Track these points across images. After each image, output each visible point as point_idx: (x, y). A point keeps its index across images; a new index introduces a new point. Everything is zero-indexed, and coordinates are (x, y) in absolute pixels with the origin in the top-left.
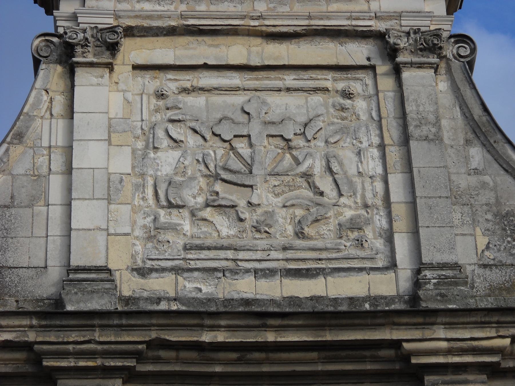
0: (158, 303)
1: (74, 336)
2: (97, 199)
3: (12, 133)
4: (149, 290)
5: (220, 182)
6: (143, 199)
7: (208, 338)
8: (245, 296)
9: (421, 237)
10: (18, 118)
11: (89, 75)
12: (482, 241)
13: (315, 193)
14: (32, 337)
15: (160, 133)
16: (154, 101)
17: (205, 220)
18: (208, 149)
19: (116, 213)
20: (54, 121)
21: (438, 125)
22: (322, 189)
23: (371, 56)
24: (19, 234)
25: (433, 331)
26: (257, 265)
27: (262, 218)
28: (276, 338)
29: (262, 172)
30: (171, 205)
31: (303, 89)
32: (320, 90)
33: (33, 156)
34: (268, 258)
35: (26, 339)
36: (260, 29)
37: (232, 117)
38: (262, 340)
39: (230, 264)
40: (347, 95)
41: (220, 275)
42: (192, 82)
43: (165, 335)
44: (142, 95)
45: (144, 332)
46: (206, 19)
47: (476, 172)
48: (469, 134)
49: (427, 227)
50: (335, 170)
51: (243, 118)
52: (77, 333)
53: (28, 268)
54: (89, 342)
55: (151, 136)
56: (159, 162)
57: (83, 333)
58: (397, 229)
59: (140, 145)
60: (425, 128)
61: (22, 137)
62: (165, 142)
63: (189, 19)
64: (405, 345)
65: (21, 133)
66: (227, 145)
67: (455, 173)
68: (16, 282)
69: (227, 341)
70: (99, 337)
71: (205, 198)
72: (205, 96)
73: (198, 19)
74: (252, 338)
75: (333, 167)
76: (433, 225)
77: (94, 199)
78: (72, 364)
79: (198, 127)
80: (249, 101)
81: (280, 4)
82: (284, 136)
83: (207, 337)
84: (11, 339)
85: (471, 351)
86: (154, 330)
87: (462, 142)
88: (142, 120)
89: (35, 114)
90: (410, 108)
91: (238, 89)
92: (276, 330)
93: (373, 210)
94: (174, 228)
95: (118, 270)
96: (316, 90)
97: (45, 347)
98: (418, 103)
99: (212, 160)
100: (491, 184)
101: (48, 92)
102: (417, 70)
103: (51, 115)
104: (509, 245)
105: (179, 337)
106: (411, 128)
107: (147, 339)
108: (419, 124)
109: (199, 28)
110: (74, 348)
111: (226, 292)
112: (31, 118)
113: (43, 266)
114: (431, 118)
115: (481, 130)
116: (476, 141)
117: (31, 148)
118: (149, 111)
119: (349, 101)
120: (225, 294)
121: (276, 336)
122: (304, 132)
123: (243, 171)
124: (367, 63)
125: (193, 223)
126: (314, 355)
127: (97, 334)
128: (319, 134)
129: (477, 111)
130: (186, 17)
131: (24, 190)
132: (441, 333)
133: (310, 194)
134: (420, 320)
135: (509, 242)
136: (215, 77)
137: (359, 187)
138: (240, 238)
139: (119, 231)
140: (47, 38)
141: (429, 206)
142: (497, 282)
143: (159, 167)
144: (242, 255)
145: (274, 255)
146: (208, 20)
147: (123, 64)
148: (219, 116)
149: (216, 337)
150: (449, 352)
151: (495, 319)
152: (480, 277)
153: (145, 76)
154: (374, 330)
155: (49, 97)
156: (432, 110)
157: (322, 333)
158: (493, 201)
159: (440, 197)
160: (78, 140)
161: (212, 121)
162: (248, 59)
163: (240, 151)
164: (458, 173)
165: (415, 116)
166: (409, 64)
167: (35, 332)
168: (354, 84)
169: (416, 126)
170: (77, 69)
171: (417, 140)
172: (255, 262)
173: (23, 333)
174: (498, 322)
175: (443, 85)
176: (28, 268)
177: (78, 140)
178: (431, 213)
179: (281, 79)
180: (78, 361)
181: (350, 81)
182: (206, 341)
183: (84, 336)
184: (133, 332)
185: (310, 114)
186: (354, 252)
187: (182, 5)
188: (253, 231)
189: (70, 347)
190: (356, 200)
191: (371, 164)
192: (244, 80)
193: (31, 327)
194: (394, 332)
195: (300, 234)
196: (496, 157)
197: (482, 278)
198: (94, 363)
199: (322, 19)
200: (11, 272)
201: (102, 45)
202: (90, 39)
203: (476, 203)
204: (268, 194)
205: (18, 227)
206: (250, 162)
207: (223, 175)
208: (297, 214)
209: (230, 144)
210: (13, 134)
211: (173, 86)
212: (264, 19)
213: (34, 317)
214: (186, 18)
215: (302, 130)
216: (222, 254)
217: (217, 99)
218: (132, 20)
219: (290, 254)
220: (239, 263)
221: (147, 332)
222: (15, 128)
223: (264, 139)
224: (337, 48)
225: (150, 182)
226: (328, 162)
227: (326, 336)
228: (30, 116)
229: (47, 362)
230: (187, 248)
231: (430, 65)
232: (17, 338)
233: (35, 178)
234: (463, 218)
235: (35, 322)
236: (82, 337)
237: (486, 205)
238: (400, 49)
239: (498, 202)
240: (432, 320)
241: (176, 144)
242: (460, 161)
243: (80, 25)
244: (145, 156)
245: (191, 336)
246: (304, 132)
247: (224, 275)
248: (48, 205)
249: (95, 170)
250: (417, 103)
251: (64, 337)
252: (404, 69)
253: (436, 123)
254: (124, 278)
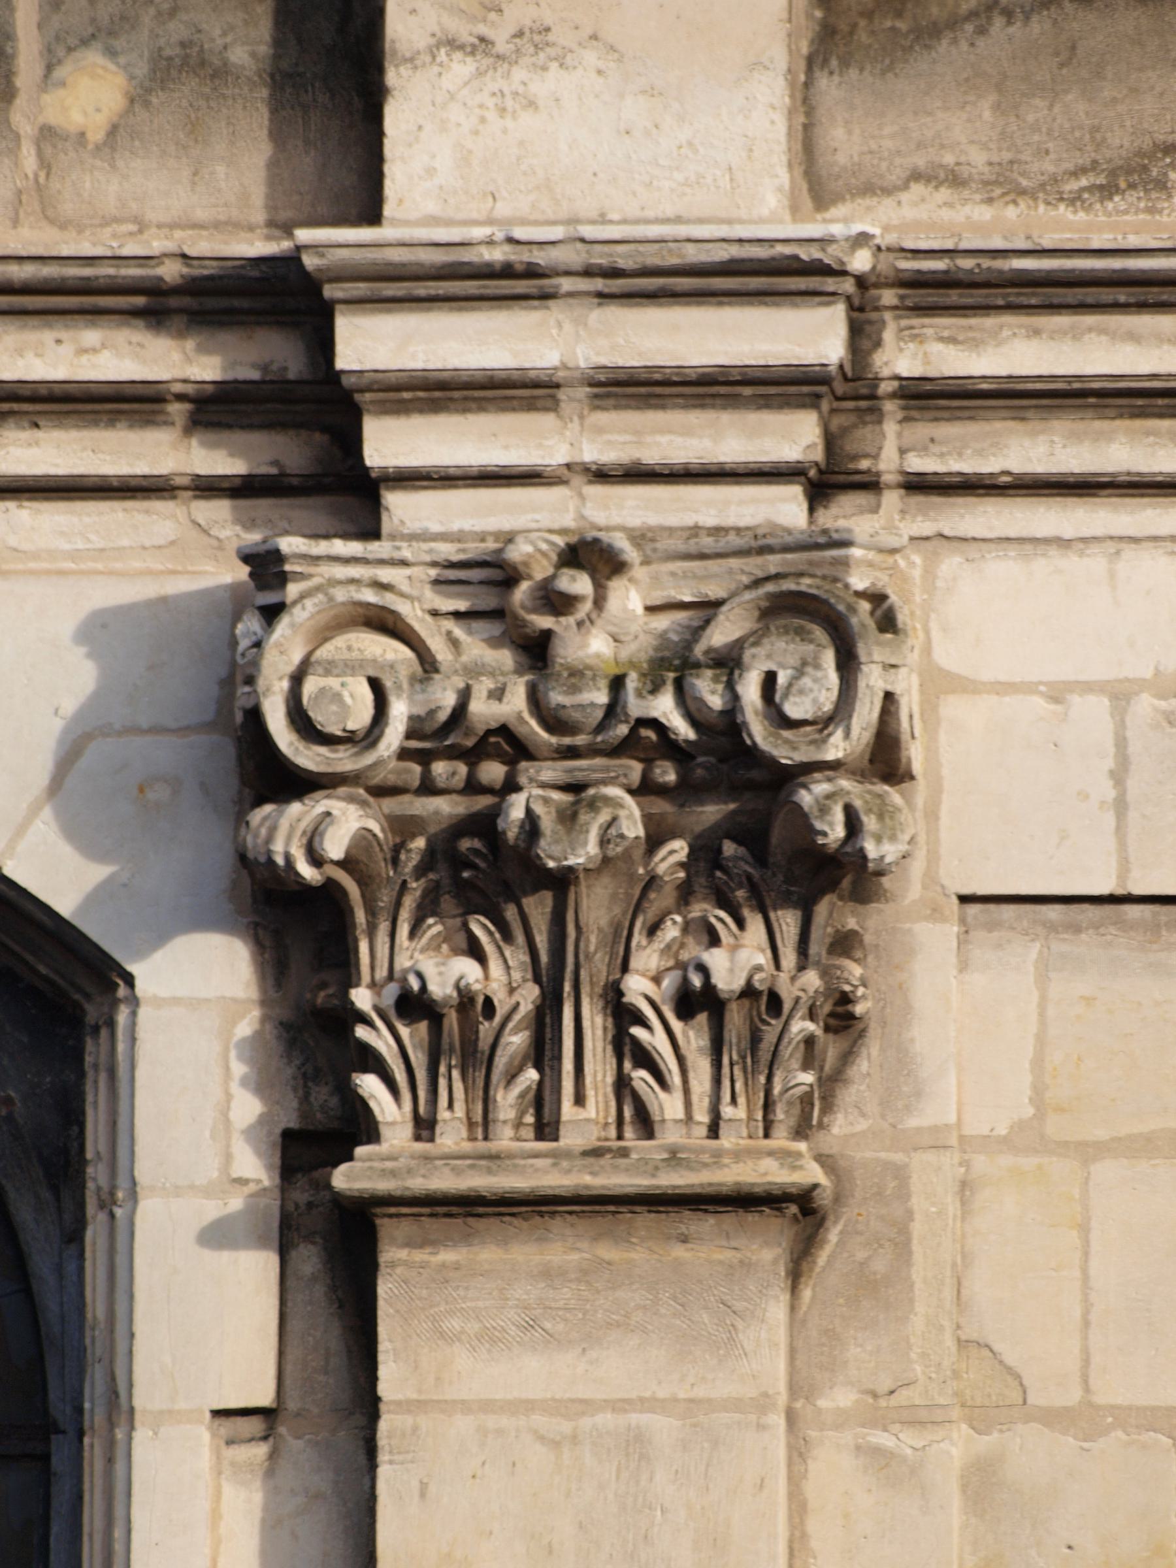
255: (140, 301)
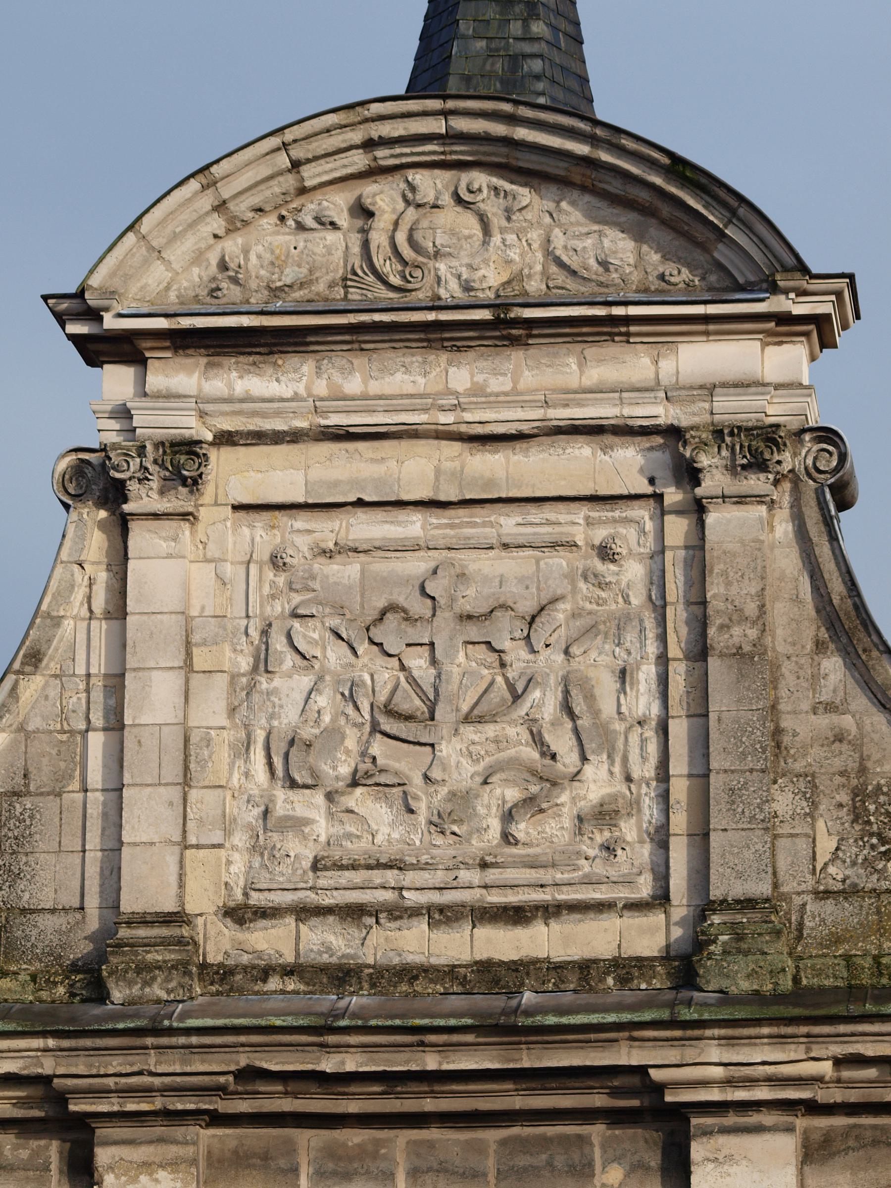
0: (265, 980)
1: (116, 1064)
2: (167, 784)
3: (21, 653)
4: (251, 951)
5: (378, 736)
6: (247, 774)
7: (330, 1065)
8: (410, 958)
9: (712, 850)
10: (33, 622)
11: (153, 536)
12: (826, 845)
13: (543, 754)
14: (48, 1066)
15: (279, 643)
16: (270, 574)
17: (350, 811)
18: (361, 670)
19: (199, 805)
20: (94, 624)
21: (760, 623)
22: (554, 748)
23: (657, 474)
24: (38, 846)
25: (699, 1051)
26: (436, 898)
27: (449, 807)
28: (440, 1064)
29: (452, 717)
30: (293, 784)
31: (533, 545)
32: (563, 545)
33: (61, 693)
34: (455, 884)
35: (40, 1071)
36: (455, 429)
37: (406, 605)
38: (418, 1068)
39: (388, 896)
40: (606, 553)
41: (371, 921)
42: (337, 534)
43: (261, 1060)
44: (249, 562)
45: (228, 1056)
46: (359, 414)
47: (830, 708)
48: (823, 629)
49: (722, 830)
50: (577, 711)
51: (421, 607)
52: (120, 1059)
53: (53, 911)
54: (140, 1073)
55: (263, 647)
56: (276, 700)
57: (130, 1058)
58: (675, 827)
59: (245, 663)
60: (736, 631)
61: (40, 660)
62: (290, 660)
63: (330, 414)
64: (652, 1072)
65: (39, 652)
66: (394, 662)
67: (788, 713)
68: (33, 938)
69: (361, 1070)
70: (156, 1065)
71: (353, 765)
72: (358, 562)
73: (345, 414)
74: (401, 1065)
75: (574, 705)
76: (734, 826)
77: (160, 784)
78: (116, 1108)
79: (344, 630)
80: (435, 572)
81: (495, 374)
82: (493, 644)
83: (328, 1064)
84: (16, 1071)
85: (764, 1081)
86: (243, 1052)
87: (809, 646)
88: (248, 616)
89: (62, 613)
90: (715, 589)
91: (417, 548)
92: (439, 1051)
93: (640, 787)
94: (297, 824)
95: (201, 915)
96: (555, 545)
97: (70, 1082)
98: (730, 579)
99: (366, 695)
100: (854, 730)
101: (83, 568)
102: (735, 507)
103: (91, 611)
104: (873, 854)
105: (283, 1063)
106: (712, 631)
107: (233, 1068)
108: (727, 621)
109: (347, 431)
110: (116, 1083)
111: (379, 954)
112: (57, 621)
113: (77, 905)
114: (751, 609)
115: (843, 626)
116: (832, 646)
117: (55, 676)
118: (261, 596)
119: (612, 567)
120: (378, 957)
121: (441, 1060)
122: (528, 635)
123: (419, 714)
124: (649, 490)
125: (331, 815)
126: (315, 1048)
127: (152, 1060)
128: (555, 635)
129: (837, 587)
130: (324, 409)
131: (45, 761)
132: (715, 1053)
133: (536, 755)
134: (678, 1033)
135: (873, 847)
136: (377, 523)
137: (620, 744)
138: (409, 844)
139: (203, 841)
140: (82, 456)
141: (730, 789)
142: (844, 927)
143: (277, 710)
144: (410, 878)
145: (465, 875)
146: (363, 414)
147: (216, 504)
148: (381, 603)
149: (343, 1063)
150: (729, 1082)
151: (804, 1030)
152: (814, 918)
153: (255, 524)
154: (601, 1049)
155: (87, 577)
156: (753, 591)
157: (515, 1054)
158: (853, 766)
159: (751, 771)
160: (134, 670)
161: (369, 615)
162: (436, 488)
163: (416, 673)
164: (795, 712)
165: (721, 606)
166: (717, 498)
167: (53, 1058)
168: (624, 531)
169: (722, 627)
170: (132, 525)
171: (721, 655)
172: (432, 891)
173: (35, 1060)
174: (808, 1036)
175: (784, 529)
176: (53, 911)
177: (134, 670)
178: (733, 802)
179: (491, 525)
180: (125, 1102)
181: (618, 525)
182: (328, 1071)
183: (131, 1065)
184: (210, 1056)
185: (542, 594)
186: (599, 869)
187: (319, 380)
188: (432, 831)
189: (110, 1082)
190: (612, 768)
191: (643, 701)
192: (429, 527)
193: (46, 1050)
194: (635, 1052)
195: (507, 838)
196: (866, 678)
197: (817, 919)
198: (151, 1105)
199: (567, 405)
200: (25, 920)
201: (175, 477)
202: (151, 467)
203: (823, 771)
204: (462, 759)
205: (36, 833)
206: (432, 698)
207: (384, 723)
208: (508, 798)
209: (400, 659)
210: (25, 656)
211: (303, 543)
212: (463, 410)
213: (376, 139)
214: (325, 413)
215: (526, 632)
216: (378, 877)
217: (381, 566)
218: (228, 418)
219: (492, 875)
220: (405, 893)
221: (234, 1056)
222: (27, 643)
223: (458, 651)
224: (596, 458)
225: (260, 736)
226: (567, 693)
227: (522, 1059)
228: (52, 618)
229: (76, 1104)
230: (316, 866)
231: (760, 499)
232: (25, 1069)
233: (64, 737)
234: (794, 802)
235: (51, 1043)
236: (128, 1067)
237: (842, 774)
238: (704, 469)
239: (862, 770)
240: (697, 1033)
241: (305, 662)
242: (802, 687)
243: (138, 430)
244: (250, 689)
245: (303, 1063)
246: (528, 635)
247: (377, 922)
248: (86, 791)
249: (163, 727)
250: (727, 578)
251: (99, 1066)
252: (711, 507)
253: (758, 618)
254: (212, 931)
255: (194, 185)
